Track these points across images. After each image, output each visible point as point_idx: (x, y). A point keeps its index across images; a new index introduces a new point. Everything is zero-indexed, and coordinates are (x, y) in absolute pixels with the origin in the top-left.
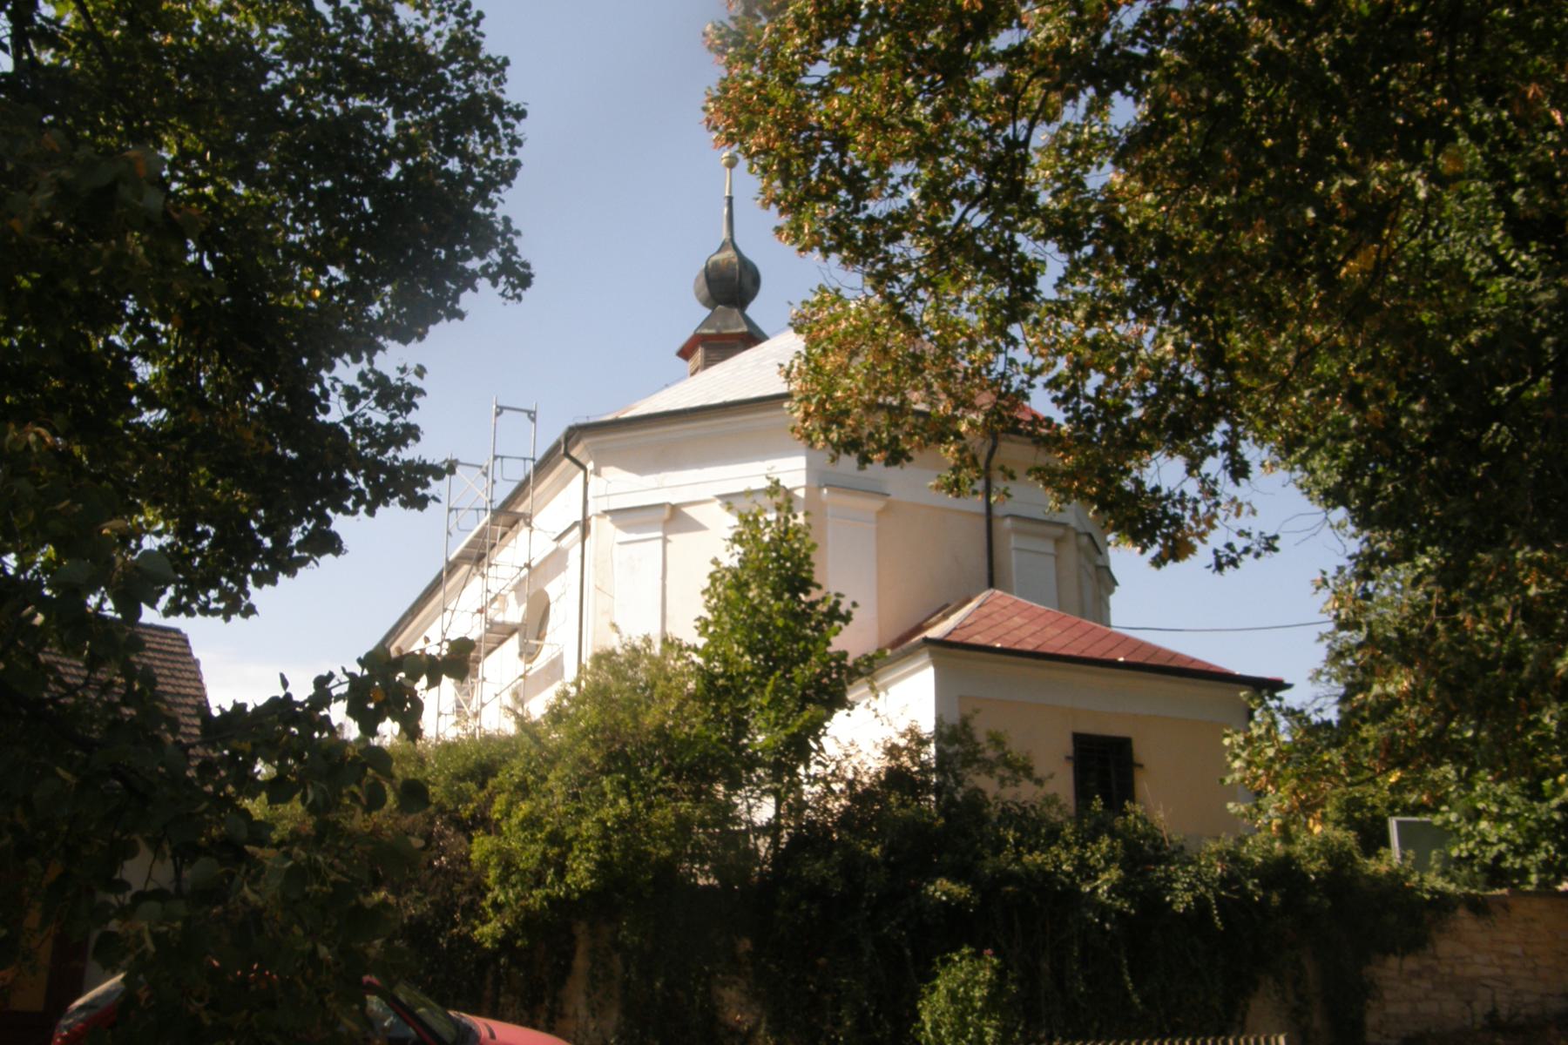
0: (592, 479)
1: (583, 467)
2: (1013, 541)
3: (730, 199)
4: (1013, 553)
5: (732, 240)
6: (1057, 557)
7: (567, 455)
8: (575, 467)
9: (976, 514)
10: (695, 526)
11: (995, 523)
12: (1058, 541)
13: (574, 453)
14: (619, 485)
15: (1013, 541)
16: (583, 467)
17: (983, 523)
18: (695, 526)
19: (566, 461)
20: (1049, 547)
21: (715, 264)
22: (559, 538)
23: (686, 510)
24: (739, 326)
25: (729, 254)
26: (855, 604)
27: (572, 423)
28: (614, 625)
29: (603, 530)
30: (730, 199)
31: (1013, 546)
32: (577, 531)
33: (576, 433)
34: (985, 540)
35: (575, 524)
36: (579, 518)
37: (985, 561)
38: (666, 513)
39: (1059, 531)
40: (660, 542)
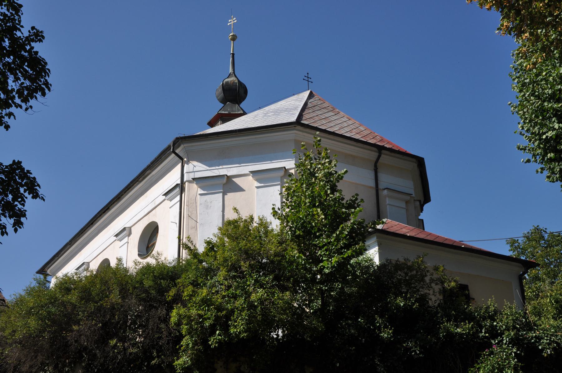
0: (186, 166)
1: (182, 159)
2: (388, 201)
3: (233, 54)
4: (388, 206)
5: (234, 73)
6: (407, 210)
7: (174, 152)
8: (178, 158)
9: (371, 187)
10: (239, 189)
11: (380, 192)
12: (407, 202)
13: (177, 151)
14: (197, 169)
15: (388, 201)
16: (182, 159)
17: (374, 192)
18: (239, 189)
19: (173, 155)
20: (403, 205)
21: (227, 83)
22: (77, 269)
23: (234, 180)
24: (239, 111)
25: (233, 79)
26: (362, 200)
27: (178, 136)
28: (235, 209)
29: (193, 190)
30: (233, 54)
31: (388, 202)
32: (178, 189)
33: (178, 141)
34: (375, 201)
35: (177, 185)
36: (179, 182)
37: (376, 209)
38: (225, 180)
39: (408, 198)
40: (221, 194)
